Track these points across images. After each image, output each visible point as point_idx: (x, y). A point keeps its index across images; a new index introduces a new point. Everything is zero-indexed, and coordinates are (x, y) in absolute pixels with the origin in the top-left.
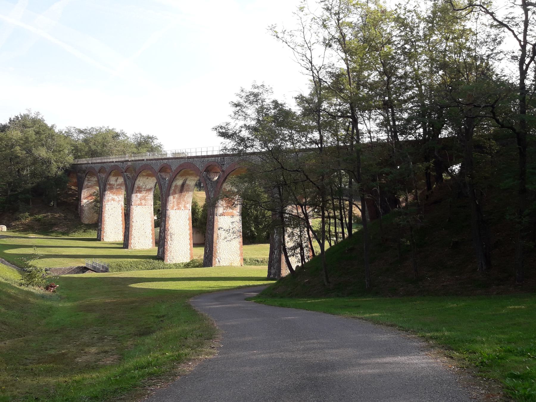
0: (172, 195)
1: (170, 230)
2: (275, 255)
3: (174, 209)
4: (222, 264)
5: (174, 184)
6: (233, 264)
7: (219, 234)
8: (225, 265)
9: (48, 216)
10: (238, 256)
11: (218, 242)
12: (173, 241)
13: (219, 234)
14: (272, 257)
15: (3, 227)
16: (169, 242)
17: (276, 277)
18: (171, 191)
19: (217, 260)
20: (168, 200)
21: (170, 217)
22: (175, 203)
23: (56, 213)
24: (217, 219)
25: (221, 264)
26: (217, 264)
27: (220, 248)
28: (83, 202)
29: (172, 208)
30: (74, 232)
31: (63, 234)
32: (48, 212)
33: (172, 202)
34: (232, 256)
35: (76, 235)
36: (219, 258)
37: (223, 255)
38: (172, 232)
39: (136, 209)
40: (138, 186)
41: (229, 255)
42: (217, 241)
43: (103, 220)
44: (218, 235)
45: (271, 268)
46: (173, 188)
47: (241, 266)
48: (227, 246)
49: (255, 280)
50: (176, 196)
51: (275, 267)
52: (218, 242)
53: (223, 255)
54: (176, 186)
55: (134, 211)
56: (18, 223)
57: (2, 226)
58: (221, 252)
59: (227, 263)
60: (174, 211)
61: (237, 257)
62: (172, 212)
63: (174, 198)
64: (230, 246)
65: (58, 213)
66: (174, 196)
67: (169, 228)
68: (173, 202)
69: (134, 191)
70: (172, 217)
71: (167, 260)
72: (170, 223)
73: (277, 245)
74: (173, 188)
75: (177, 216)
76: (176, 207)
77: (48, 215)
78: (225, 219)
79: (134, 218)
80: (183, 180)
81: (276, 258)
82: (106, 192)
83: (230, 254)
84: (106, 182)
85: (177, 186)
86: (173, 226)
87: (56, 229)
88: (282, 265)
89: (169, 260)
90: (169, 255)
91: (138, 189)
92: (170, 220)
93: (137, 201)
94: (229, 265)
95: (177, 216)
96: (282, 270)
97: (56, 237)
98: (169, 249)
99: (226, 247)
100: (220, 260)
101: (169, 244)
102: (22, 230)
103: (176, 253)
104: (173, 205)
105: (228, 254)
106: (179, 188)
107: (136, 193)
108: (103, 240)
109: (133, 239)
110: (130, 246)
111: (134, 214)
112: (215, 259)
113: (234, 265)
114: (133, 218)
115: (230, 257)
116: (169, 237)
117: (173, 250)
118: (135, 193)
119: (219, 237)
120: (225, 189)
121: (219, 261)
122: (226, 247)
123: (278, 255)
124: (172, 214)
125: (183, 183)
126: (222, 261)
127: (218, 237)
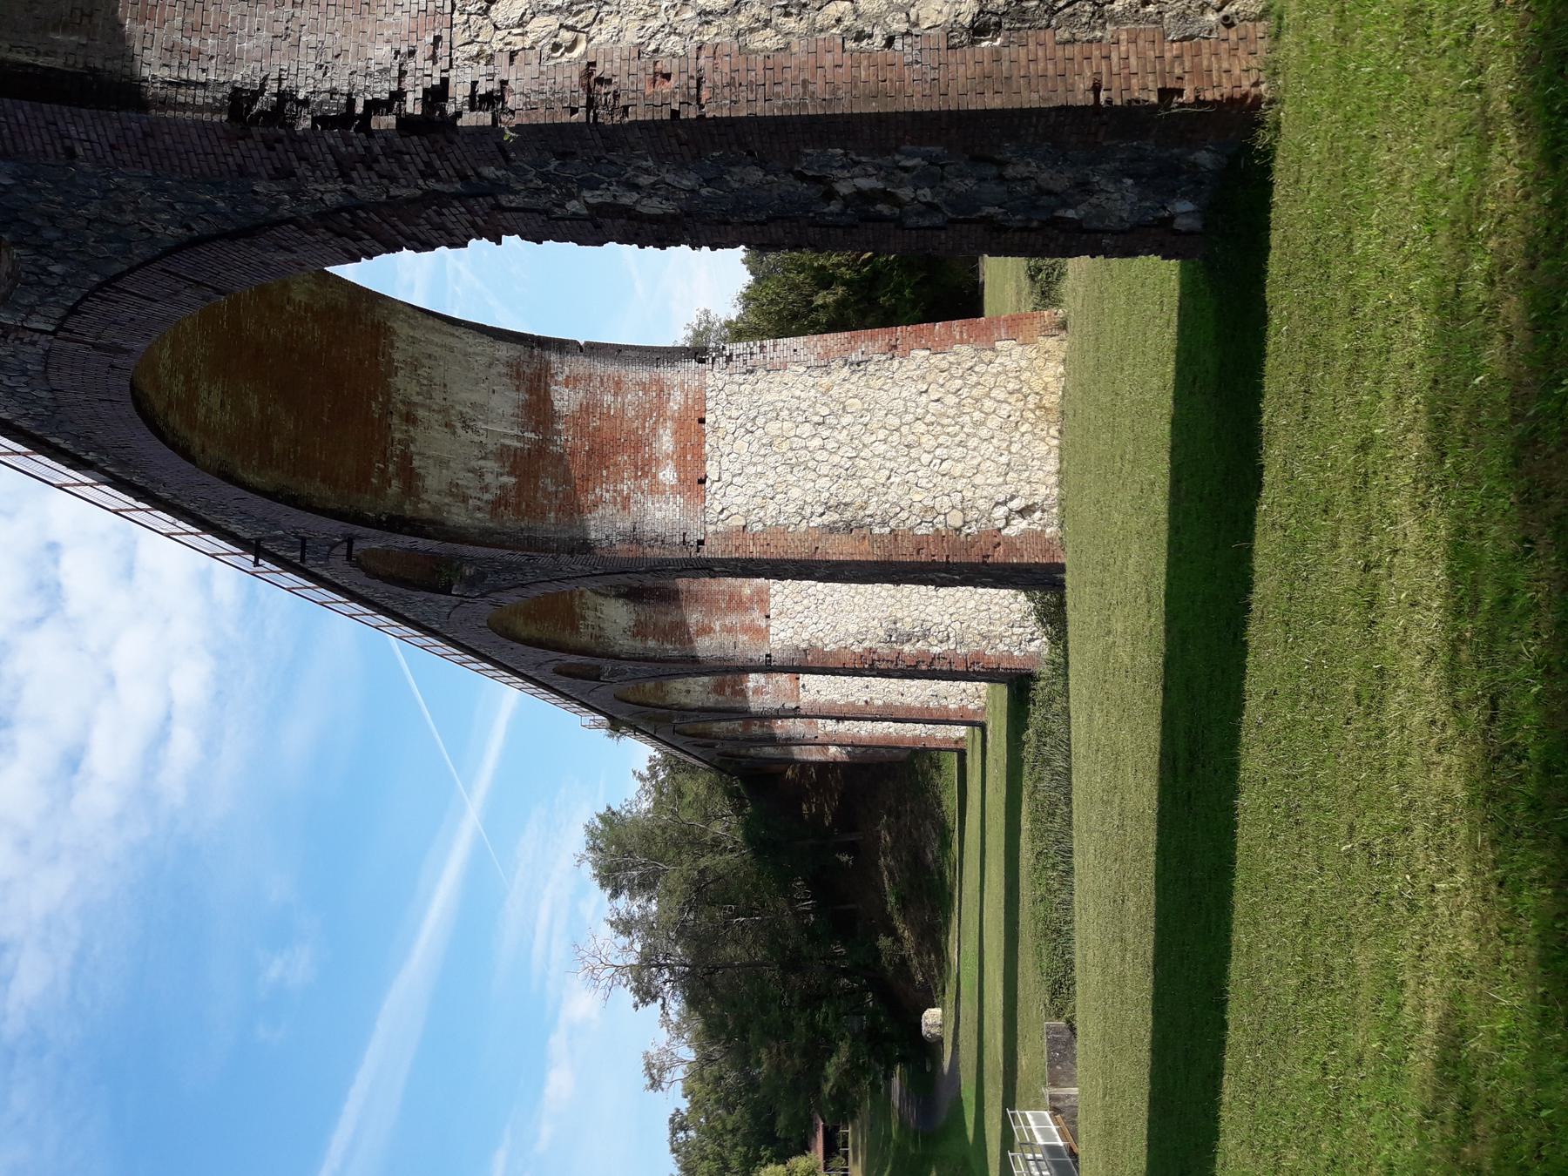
0: (690, 641)
1: (873, 645)
2: (905, 193)
3: (763, 623)
4: (1042, 483)
5: (626, 644)
6: (1052, 400)
7: (831, 517)
8: (1052, 465)
9: (887, 867)
10: (989, 354)
11: (884, 523)
12: (927, 625)
13: (827, 519)
14: (938, 220)
15: (930, 1021)
16: (936, 650)
17: (1204, 158)
18: (672, 650)
19: (1019, 525)
20: (720, 659)
21: (804, 646)
22: (732, 619)
23: (879, 838)
24: (726, 536)
25: (1043, 491)
26: (1046, 524)
27: (927, 509)
28: (837, 754)
29: (762, 634)
30: (940, 805)
31: (946, 845)
32: (877, 866)
33: (728, 640)
34: (988, 405)
35: (950, 802)
36: (1000, 512)
37: (978, 480)
38: (882, 633)
39: (812, 692)
40: (715, 691)
41: (984, 433)
42: (876, 530)
43: (883, 743)
44: (831, 529)
45: (1077, 227)
46: (651, 643)
47: (1063, 326)
48: (914, 453)
49: (1243, 525)
50: (694, 618)
51: (1058, 180)
52: (884, 523)
53: (978, 480)
54: (639, 630)
55: (822, 699)
56: (915, 962)
57: (923, 1024)
58: (957, 498)
59: (1043, 448)
60: (775, 625)
61: (994, 369)
62: (782, 635)
63: (706, 630)
64: (920, 427)
65: (879, 832)
66: (698, 634)
67: (858, 649)
68: (730, 630)
69: (736, 703)
70: (806, 636)
71: (1030, 657)
72: (832, 646)
73: (756, 175)
74: (651, 643)
75: (799, 608)
76: (756, 616)
77: (887, 867)
78: (726, 477)
79: (852, 699)
80: (600, 600)
81: (921, 178)
82: (778, 731)
83: (976, 424)
84: (737, 739)
85: (638, 623)
86: (853, 629)
87: (930, 856)
88: (1031, 99)
89: (1033, 647)
90: (1001, 647)
91: (728, 691)
92: (820, 644)
93: (778, 690)
94: (1053, 432)
95: (799, 608)
96: (1114, 95)
97: (955, 873)
98: (974, 647)
99: (926, 458)
100: (1016, 504)
101: (945, 647)
102: (937, 957)
103: (995, 608)
104: (747, 630)
105: (973, 443)
106: (647, 612)
107: (743, 693)
108: (961, 739)
109: (944, 702)
110: (975, 712)
111: (836, 697)
112: (1010, 542)
113: (1056, 387)
114: (853, 704)
115: (993, 422)
116: (907, 648)
117: (974, 624)
118: (745, 697)
119: (848, 515)
120: (496, 504)
121: (1024, 512)
122: (926, 458)
123: (886, 161)
124: (789, 633)
125: (618, 596)
126: (1027, 489)
127: (848, 528)
